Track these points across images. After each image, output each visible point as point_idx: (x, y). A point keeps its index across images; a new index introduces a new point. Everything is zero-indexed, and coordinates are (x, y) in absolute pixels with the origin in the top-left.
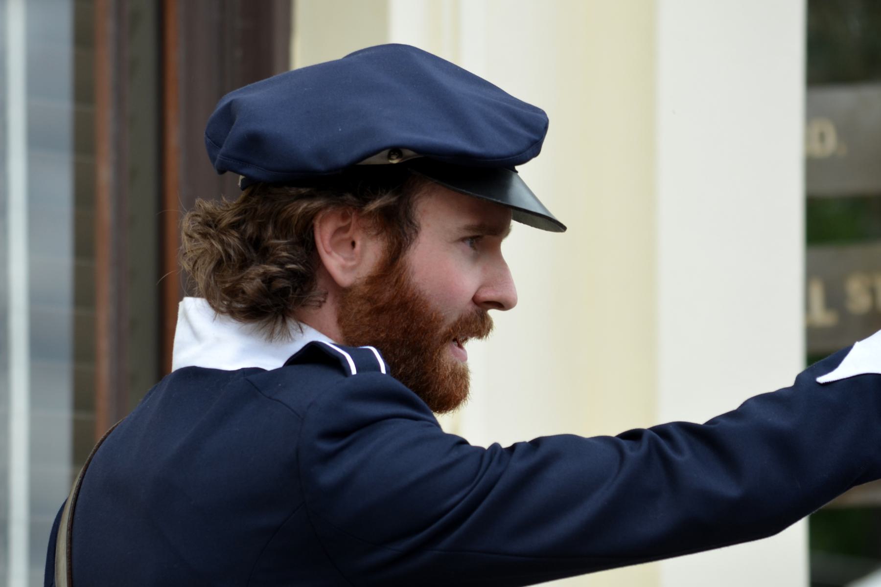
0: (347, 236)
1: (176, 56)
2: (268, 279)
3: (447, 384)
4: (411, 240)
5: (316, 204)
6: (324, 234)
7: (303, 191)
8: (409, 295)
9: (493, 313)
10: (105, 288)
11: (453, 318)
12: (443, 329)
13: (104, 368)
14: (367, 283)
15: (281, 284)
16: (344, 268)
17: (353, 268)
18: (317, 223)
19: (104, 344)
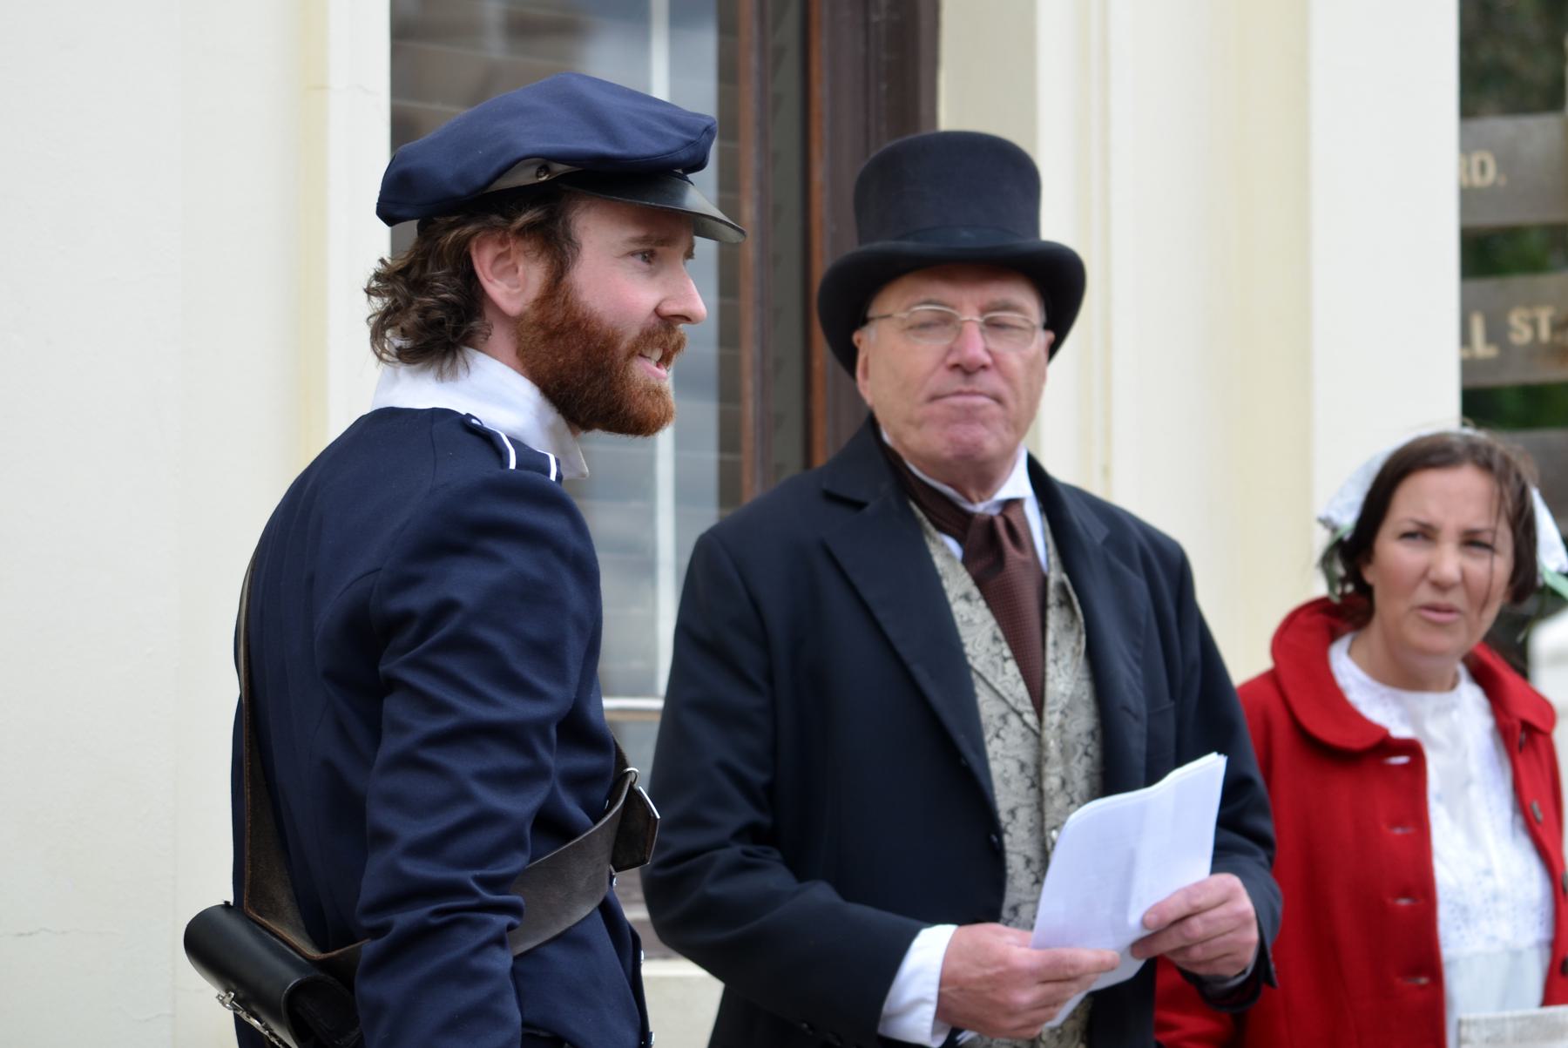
0: (510, 263)
1: (820, 91)
2: (424, 312)
3: (640, 400)
4: (574, 259)
5: (469, 229)
6: (484, 261)
7: (453, 219)
8: (580, 315)
9: (682, 327)
10: (750, 327)
11: (634, 332)
12: (624, 345)
13: (750, 408)
14: (539, 308)
15: (438, 314)
16: (509, 296)
17: (519, 295)
18: (474, 253)
19: (749, 385)
